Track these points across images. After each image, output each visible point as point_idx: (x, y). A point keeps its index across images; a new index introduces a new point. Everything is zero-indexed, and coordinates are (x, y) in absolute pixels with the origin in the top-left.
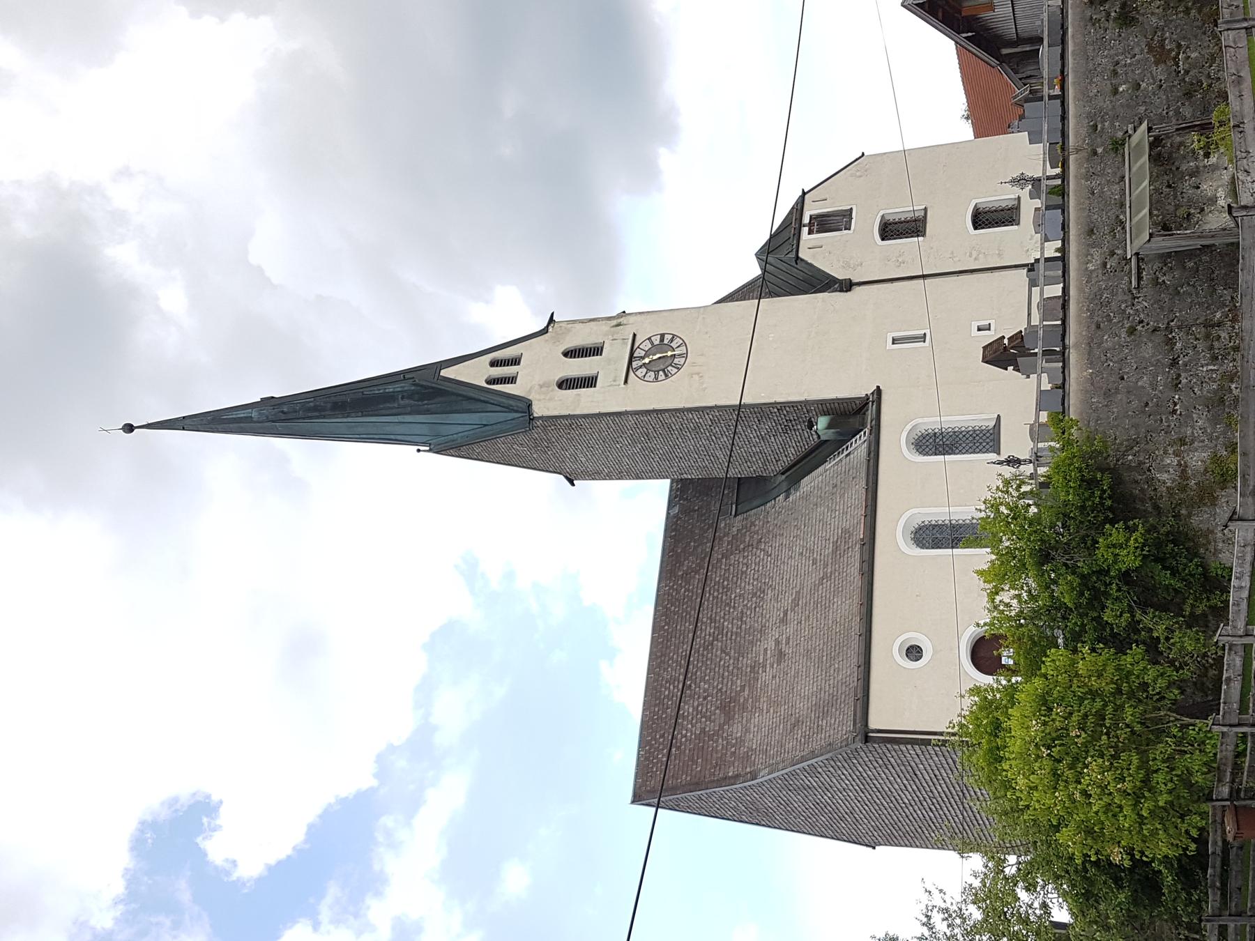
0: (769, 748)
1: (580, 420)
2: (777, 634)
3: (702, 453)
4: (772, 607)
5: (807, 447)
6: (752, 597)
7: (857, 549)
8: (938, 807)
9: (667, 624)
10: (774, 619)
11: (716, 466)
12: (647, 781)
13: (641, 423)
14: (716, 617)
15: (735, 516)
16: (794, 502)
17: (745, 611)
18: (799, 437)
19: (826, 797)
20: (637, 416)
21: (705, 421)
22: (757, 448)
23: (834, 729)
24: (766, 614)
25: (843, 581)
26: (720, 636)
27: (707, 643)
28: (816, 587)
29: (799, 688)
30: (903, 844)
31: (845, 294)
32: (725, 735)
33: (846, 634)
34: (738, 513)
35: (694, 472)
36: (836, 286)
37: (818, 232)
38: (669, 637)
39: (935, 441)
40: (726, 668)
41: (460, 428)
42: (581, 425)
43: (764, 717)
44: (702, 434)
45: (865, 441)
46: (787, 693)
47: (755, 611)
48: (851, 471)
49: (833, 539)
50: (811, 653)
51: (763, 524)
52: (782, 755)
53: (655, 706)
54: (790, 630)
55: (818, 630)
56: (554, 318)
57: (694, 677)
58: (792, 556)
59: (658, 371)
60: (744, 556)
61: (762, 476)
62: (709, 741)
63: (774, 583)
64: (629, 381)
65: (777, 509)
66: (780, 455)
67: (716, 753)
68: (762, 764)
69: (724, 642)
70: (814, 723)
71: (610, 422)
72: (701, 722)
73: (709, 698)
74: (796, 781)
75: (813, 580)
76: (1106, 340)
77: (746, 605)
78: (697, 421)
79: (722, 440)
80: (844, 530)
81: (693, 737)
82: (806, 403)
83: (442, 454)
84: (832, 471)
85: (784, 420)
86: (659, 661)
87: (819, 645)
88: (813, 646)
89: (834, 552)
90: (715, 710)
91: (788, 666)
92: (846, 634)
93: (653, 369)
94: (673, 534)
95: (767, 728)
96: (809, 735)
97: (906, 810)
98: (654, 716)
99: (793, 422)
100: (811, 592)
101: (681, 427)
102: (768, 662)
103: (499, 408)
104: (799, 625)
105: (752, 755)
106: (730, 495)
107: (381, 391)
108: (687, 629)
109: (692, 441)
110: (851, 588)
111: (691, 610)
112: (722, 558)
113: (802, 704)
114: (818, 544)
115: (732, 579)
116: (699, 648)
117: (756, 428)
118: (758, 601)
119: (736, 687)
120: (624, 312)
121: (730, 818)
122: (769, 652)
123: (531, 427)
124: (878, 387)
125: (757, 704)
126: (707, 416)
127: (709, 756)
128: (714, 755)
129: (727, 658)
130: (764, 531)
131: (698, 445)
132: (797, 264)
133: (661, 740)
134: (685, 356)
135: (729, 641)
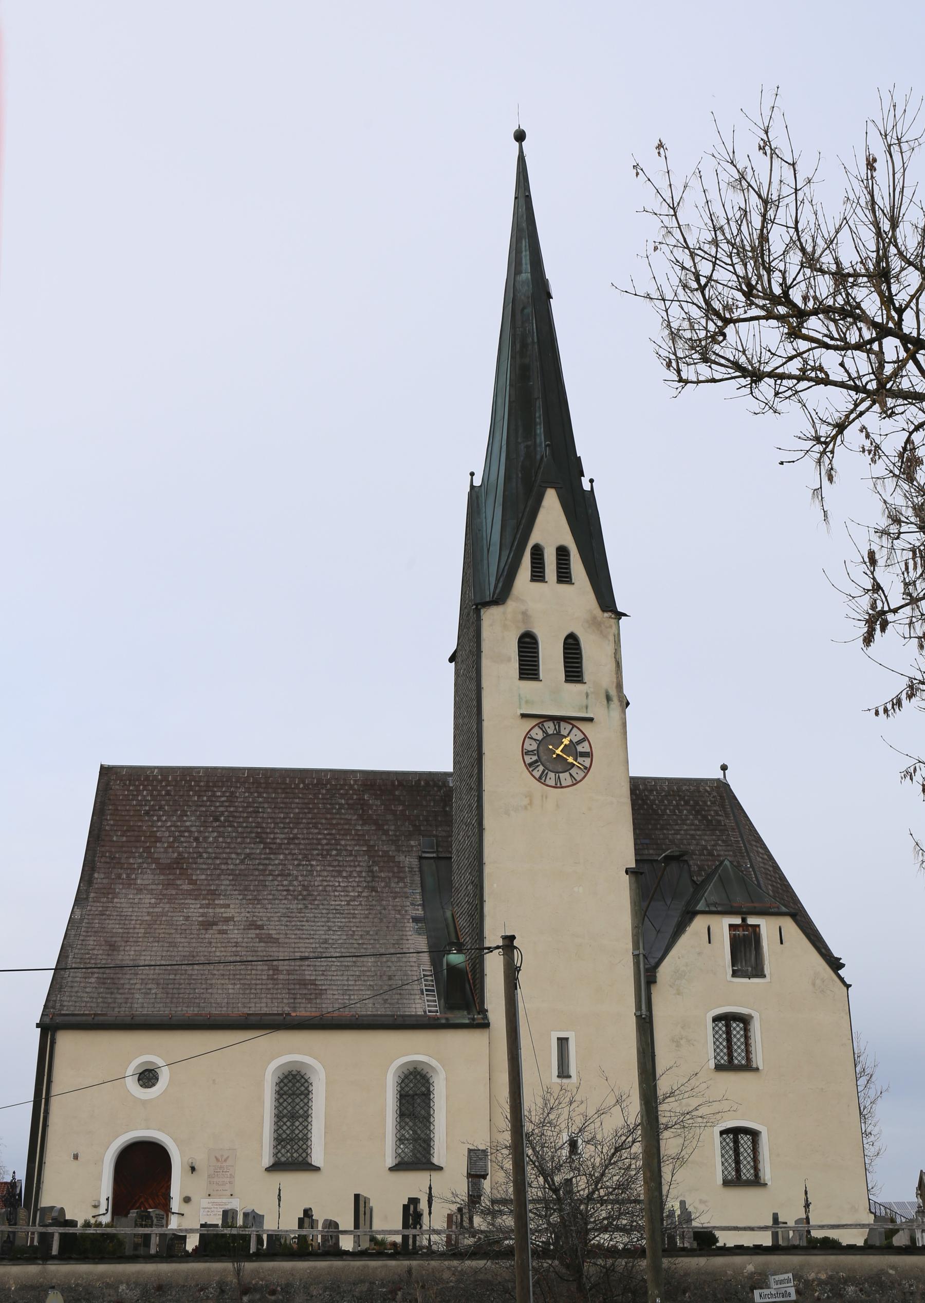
26: (268, 851)
64: (525, 720)
93: (541, 748)
107: (538, 420)
134: (558, 786)
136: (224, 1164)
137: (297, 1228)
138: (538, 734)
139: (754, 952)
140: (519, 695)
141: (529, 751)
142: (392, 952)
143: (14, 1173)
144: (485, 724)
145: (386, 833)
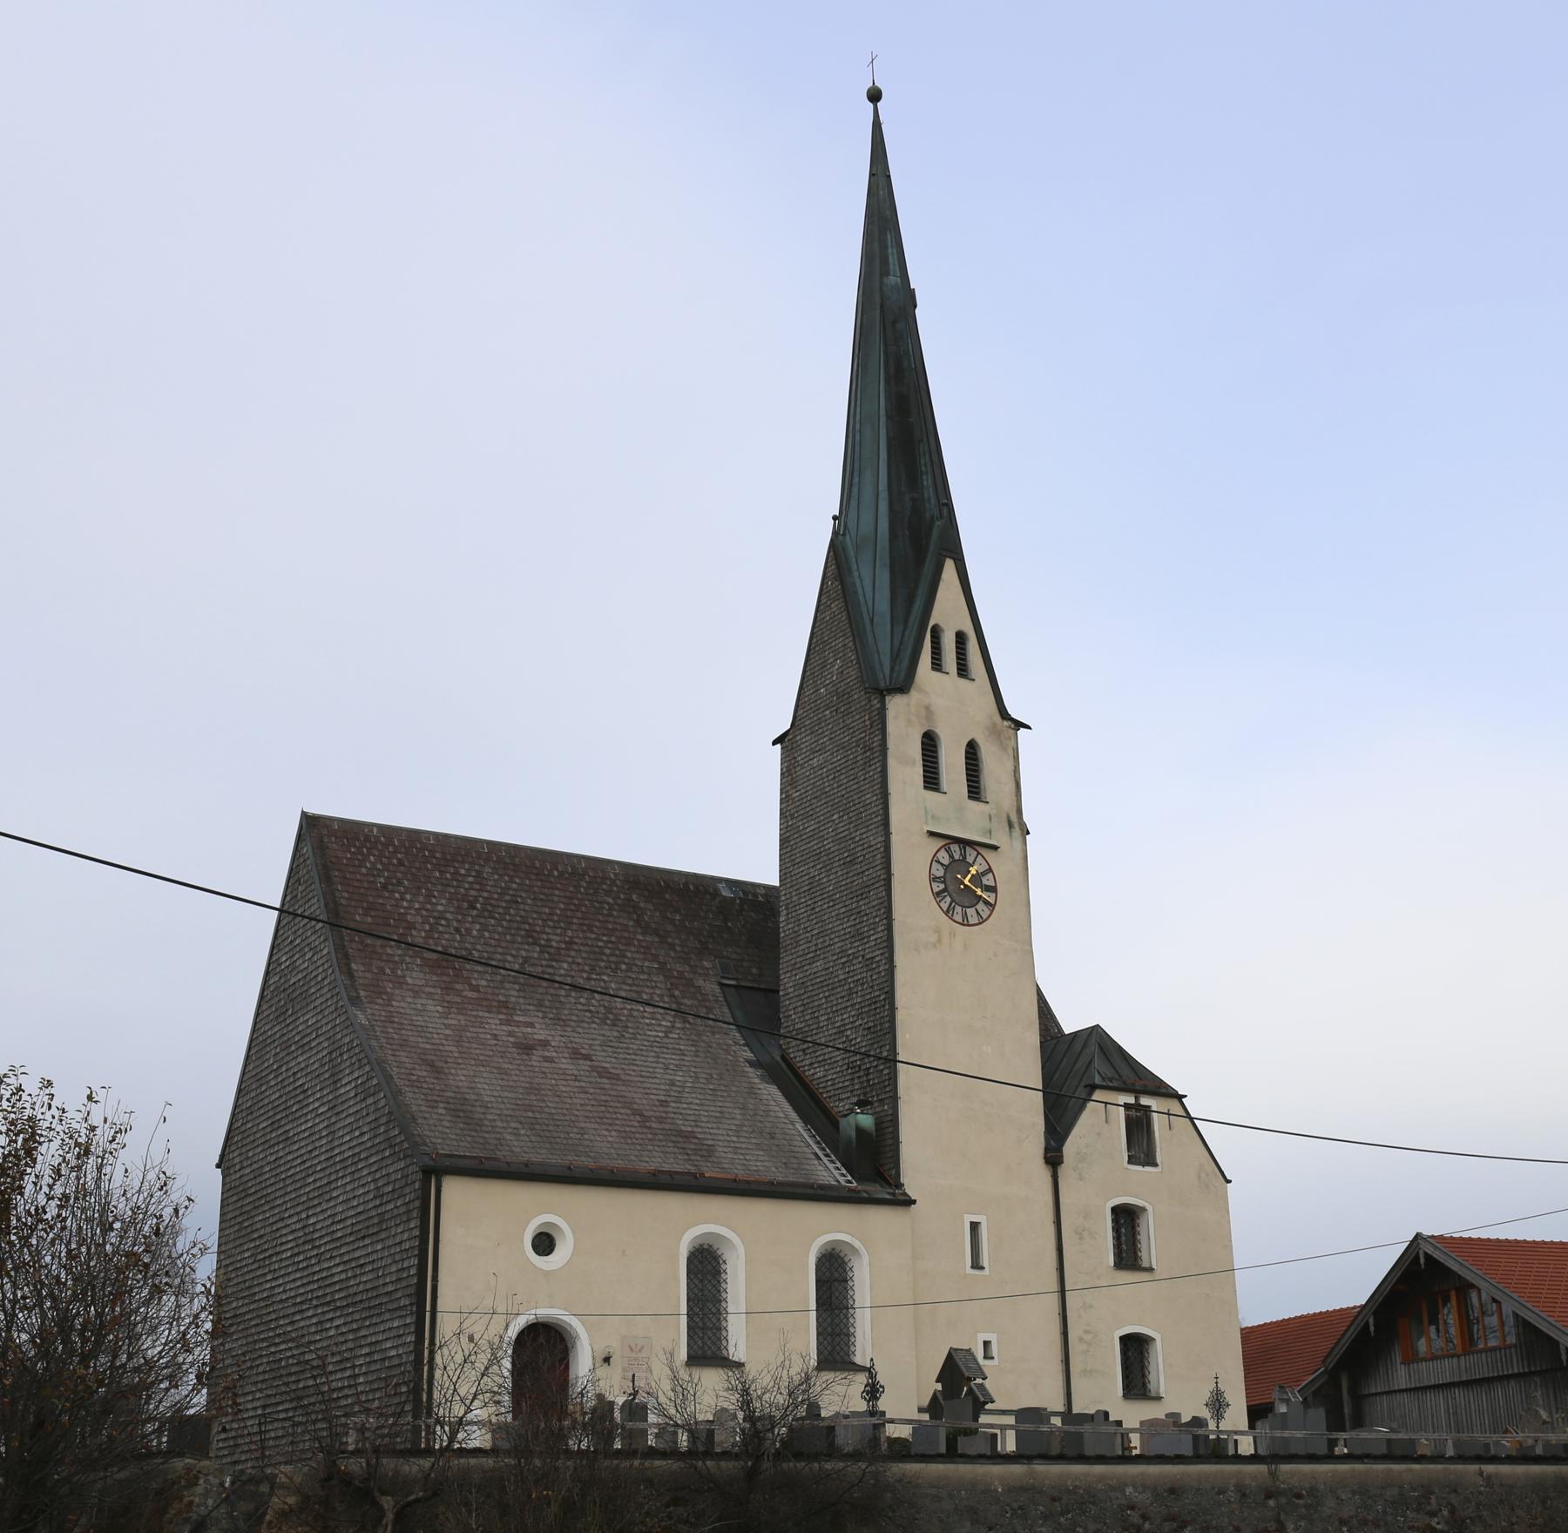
0: (395, 1025)
1: (878, 764)
2: (556, 1044)
3: (821, 940)
5: (825, 1096)
6: (605, 1007)
7: (689, 1167)
9: (561, 874)
10: (577, 1040)
11: (799, 960)
12: (336, 837)
13: (872, 854)
15: (722, 985)
18: (841, 1085)
19: (316, 1105)
20: (882, 849)
23: (435, 1126)
24: (584, 1028)
25: (641, 1145)
26: (547, 956)
29: (485, 1075)
32: (408, 960)
34: (725, 989)
35: (790, 926)
36: (1053, 1143)
37: (1128, 1120)
38: (543, 878)
39: (836, 1280)
41: (867, 582)
42: (870, 766)
44: (851, 943)
45: (838, 1181)
46: (476, 1057)
47: (587, 1011)
48: (795, 1161)
49: (699, 1133)
50: (535, 1094)
52: (389, 1046)
53: (444, 853)
54: (565, 1064)
55: (568, 1106)
56: (1022, 729)
57: (486, 914)
59: (944, 882)
61: (780, 1027)
63: (627, 1041)
65: (733, 1048)
66: (812, 1055)
67: (381, 946)
70: (439, 1096)
71: (875, 809)
73: (458, 936)
74: (348, 1063)
76: (1038, 1510)
78: (872, 938)
79: (840, 972)
81: (402, 911)
84: (792, 1132)
85: (868, 1066)
86: (508, 860)
87: (547, 1106)
88: (546, 1099)
89: (680, 1133)
91: (514, 1059)
94: (692, 887)
95: (423, 1024)
96: (422, 1087)
97: (295, 1219)
98: (429, 851)
100: (622, 1097)
101: (862, 914)
102: (516, 1029)
103: (896, 644)
104: (573, 1077)
105: (383, 999)
106: (749, 977)
108: (554, 905)
109: (841, 927)
110: (632, 1158)
111: (583, 912)
112: (659, 963)
113: (463, 1078)
115: (629, 977)
116: (529, 924)
117: (857, 1023)
118: (600, 1015)
119: (476, 979)
120: (1028, 833)
123: (868, 690)
124: (914, 1202)
125: (455, 1011)
126: (878, 952)
130: (700, 1028)
131: (833, 936)
132: (1086, 1086)
133: (395, 861)
136: (639, 1355)
137: (1247, 1429)
140: (925, 808)
143: (872, 1360)
144: (894, 838)
145: (672, 947)
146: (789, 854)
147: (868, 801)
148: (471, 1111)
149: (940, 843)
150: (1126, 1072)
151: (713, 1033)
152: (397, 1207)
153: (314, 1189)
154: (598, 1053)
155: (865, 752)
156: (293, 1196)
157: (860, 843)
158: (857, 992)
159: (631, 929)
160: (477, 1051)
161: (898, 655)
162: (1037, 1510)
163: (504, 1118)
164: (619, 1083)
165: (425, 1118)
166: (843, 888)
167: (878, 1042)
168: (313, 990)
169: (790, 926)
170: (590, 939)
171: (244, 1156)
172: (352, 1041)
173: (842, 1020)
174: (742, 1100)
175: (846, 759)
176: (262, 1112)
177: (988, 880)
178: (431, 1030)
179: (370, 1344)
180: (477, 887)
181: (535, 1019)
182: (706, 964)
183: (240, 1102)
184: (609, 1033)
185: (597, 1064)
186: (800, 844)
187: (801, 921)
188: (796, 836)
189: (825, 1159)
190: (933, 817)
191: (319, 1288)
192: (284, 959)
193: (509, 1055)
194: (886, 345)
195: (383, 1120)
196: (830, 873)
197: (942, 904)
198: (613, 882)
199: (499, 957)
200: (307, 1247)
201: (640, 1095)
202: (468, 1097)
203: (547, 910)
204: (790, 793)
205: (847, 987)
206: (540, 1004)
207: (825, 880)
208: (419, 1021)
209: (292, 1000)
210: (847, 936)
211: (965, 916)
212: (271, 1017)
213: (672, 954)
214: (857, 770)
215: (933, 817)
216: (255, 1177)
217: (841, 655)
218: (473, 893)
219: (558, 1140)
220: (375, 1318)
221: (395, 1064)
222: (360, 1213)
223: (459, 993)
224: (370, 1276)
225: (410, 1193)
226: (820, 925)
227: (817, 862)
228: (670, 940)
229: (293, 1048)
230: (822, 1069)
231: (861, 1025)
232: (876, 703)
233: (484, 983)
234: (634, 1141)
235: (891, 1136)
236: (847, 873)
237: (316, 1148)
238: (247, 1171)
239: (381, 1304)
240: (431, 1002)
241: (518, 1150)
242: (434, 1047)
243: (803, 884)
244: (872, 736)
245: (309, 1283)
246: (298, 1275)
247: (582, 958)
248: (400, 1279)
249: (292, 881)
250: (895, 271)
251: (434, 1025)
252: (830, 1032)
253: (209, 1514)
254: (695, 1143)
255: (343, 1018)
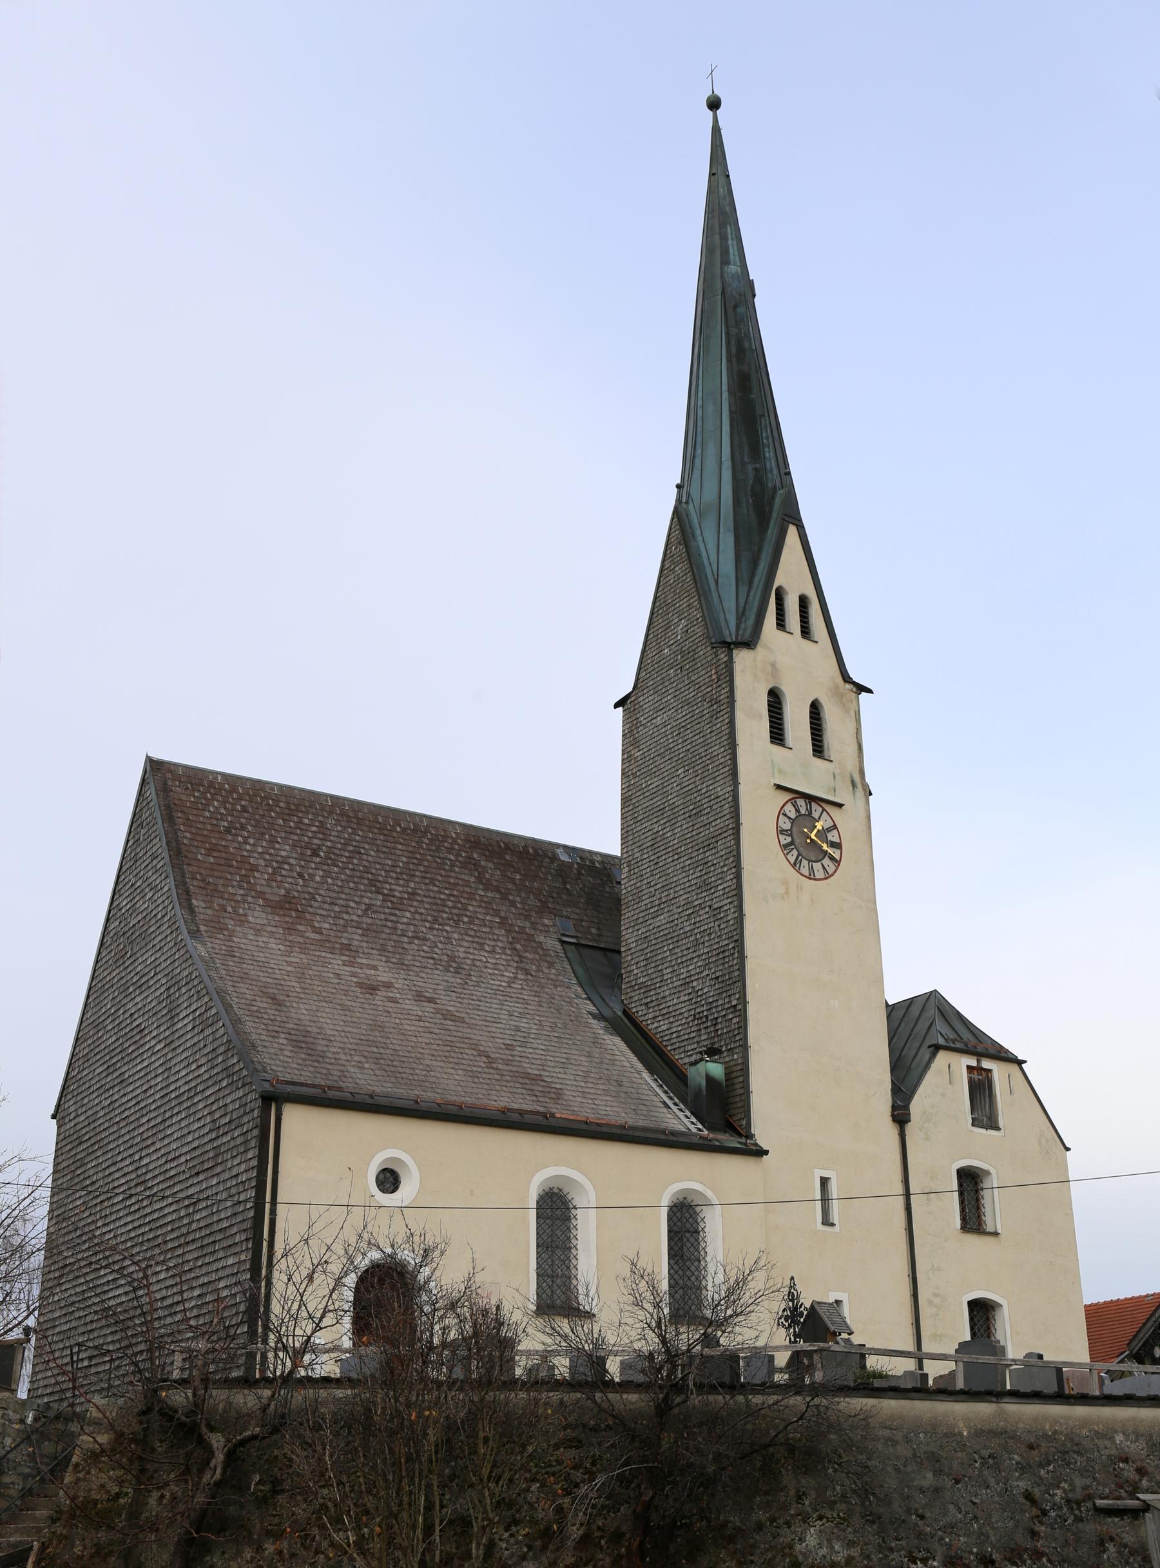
0: (236, 959)
1: (726, 716)
3: (665, 894)
4: (437, 982)
5: (669, 1048)
8: (132, 1209)
9: (404, 830)
10: (421, 984)
11: (640, 915)
12: (180, 782)
13: (719, 805)
14: (417, 901)
16: (587, 1025)
17: (428, 943)
18: (686, 1037)
19: (153, 1043)
20: (730, 799)
21: (717, 900)
22: (670, 976)
23: (276, 1055)
26: (389, 904)
27: (378, 884)
28: (475, 1046)
29: (328, 1010)
30: (60, 1159)
31: (890, 1114)
32: (250, 899)
33: (413, 1082)
35: (632, 882)
37: (971, 1082)
38: (385, 832)
40: (346, 909)
42: (717, 718)
43: (279, 958)
45: (689, 1129)
48: (643, 1108)
51: (552, 980)
52: (229, 978)
53: (288, 803)
54: (409, 1005)
58: (512, 1015)
59: (791, 835)
60: (505, 948)
62: (240, 875)
63: (470, 988)
66: (656, 1008)
68: (213, 948)
69: (381, 910)
71: (723, 760)
72: (266, 866)
74: (186, 996)
75: (483, 1043)
76: (1013, 1459)
77: (436, 946)
80: (560, 1092)
81: (245, 853)
82: (745, 1047)
83: (673, 519)
84: (640, 1081)
86: (351, 814)
88: (390, 1035)
89: (527, 1076)
90: (285, 889)
92: (413, 1082)
95: (264, 960)
97: (128, 1162)
98: (273, 800)
99: (712, 1029)
102: (359, 970)
103: (742, 601)
109: (686, 879)
110: (480, 1096)
112: (501, 918)
113: (305, 1012)
114: (536, 1053)
116: (372, 874)
117: (704, 974)
118: (444, 963)
121: (115, 904)
122: (372, 972)
124: (766, 1152)
125: (298, 950)
126: (726, 901)
127: (219, 874)
128: (221, 882)
129: (360, 913)
130: (542, 981)
132: (929, 1047)
133: (239, 807)
134: (811, 877)
135: (383, 917)
138: (790, 811)
139: (988, 1101)
141: (783, 830)
142: (918, 1045)
143: (792, 1278)
144: (743, 789)
145: (513, 904)
146: (631, 812)
147: (716, 753)
148: (313, 1043)
149: (788, 796)
150: (966, 1035)
151: (556, 986)
152: (233, 1139)
153: (148, 1129)
154: (442, 997)
155: (711, 706)
156: (127, 1138)
157: (707, 795)
158: (703, 943)
159: (473, 885)
160: (320, 988)
161: (743, 613)
162: (1011, 1459)
163: (347, 1051)
164: (465, 1025)
165: (266, 1047)
166: (688, 841)
167: (726, 991)
168: (152, 929)
169: (632, 882)
170: (433, 891)
171: (79, 1104)
172: (190, 974)
173: (688, 971)
174: (587, 1049)
175: (691, 714)
176: (98, 1057)
177: (833, 837)
178: (273, 966)
179: (202, 1285)
180: (321, 836)
181: (378, 963)
182: (546, 921)
183: (77, 1051)
184: (453, 980)
185: (439, 1006)
186: (643, 801)
187: (644, 877)
188: (638, 794)
189: (674, 1108)
190: (780, 771)
191: (151, 1230)
192: (124, 903)
193: (351, 994)
194: (727, 326)
195: (222, 1049)
196: (674, 827)
197: (789, 857)
198: (455, 841)
199: (342, 902)
200: (139, 1189)
201: (486, 1038)
202: (310, 1029)
203: (390, 862)
204: (632, 753)
205: (693, 938)
206: (383, 949)
207: (669, 834)
208: (261, 956)
209: (132, 942)
210: (693, 888)
211: (811, 869)
212: (110, 962)
213: (513, 910)
214: (703, 724)
215: (780, 771)
216: (89, 1124)
217: (685, 614)
218: (316, 841)
219: (404, 1075)
220: (207, 1258)
221: (235, 994)
222: (194, 1149)
223: (301, 934)
224: (204, 1214)
225: (249, 1122)
226: (664, 878)
227: (661, 817)
228: (511, 897)
229: (131, 989)
230: (666, 1022)
231: (708, 975)
232: (723, 657)
233: (327, 926)
234: (481, 1080)
235: (741, 1085)
236: (693, 825)
237: (151, 1087)
238: (82, 1118)
239: (215, 1242)
240: (272, 940)
241: (362, 1082)
242: (276, 981)
243: (646, 841)
244: (719, 689)
245: (140, 1226)
246: (129, 1219)
247: (425, 908)
248: (235, 1214)
249: (135, 826)
250: (735, 261)
251: (276, 962)
252: (675, 984)
253: (5, 1456)
254: (543, 1086)
255: (182, 952)
